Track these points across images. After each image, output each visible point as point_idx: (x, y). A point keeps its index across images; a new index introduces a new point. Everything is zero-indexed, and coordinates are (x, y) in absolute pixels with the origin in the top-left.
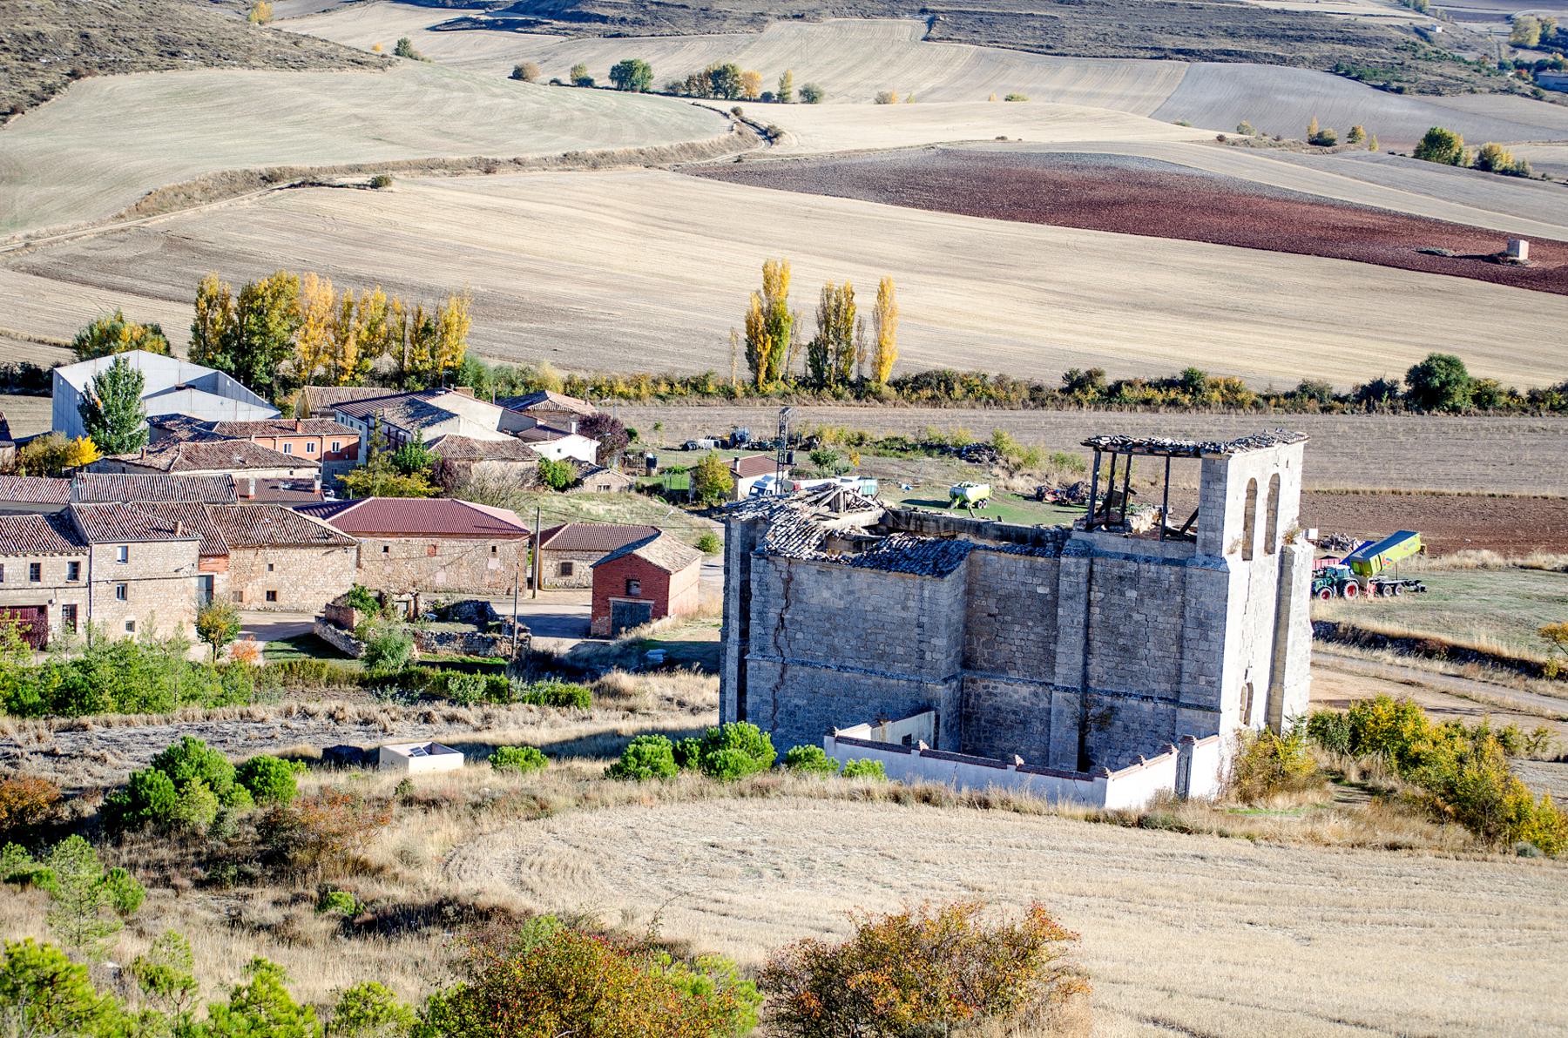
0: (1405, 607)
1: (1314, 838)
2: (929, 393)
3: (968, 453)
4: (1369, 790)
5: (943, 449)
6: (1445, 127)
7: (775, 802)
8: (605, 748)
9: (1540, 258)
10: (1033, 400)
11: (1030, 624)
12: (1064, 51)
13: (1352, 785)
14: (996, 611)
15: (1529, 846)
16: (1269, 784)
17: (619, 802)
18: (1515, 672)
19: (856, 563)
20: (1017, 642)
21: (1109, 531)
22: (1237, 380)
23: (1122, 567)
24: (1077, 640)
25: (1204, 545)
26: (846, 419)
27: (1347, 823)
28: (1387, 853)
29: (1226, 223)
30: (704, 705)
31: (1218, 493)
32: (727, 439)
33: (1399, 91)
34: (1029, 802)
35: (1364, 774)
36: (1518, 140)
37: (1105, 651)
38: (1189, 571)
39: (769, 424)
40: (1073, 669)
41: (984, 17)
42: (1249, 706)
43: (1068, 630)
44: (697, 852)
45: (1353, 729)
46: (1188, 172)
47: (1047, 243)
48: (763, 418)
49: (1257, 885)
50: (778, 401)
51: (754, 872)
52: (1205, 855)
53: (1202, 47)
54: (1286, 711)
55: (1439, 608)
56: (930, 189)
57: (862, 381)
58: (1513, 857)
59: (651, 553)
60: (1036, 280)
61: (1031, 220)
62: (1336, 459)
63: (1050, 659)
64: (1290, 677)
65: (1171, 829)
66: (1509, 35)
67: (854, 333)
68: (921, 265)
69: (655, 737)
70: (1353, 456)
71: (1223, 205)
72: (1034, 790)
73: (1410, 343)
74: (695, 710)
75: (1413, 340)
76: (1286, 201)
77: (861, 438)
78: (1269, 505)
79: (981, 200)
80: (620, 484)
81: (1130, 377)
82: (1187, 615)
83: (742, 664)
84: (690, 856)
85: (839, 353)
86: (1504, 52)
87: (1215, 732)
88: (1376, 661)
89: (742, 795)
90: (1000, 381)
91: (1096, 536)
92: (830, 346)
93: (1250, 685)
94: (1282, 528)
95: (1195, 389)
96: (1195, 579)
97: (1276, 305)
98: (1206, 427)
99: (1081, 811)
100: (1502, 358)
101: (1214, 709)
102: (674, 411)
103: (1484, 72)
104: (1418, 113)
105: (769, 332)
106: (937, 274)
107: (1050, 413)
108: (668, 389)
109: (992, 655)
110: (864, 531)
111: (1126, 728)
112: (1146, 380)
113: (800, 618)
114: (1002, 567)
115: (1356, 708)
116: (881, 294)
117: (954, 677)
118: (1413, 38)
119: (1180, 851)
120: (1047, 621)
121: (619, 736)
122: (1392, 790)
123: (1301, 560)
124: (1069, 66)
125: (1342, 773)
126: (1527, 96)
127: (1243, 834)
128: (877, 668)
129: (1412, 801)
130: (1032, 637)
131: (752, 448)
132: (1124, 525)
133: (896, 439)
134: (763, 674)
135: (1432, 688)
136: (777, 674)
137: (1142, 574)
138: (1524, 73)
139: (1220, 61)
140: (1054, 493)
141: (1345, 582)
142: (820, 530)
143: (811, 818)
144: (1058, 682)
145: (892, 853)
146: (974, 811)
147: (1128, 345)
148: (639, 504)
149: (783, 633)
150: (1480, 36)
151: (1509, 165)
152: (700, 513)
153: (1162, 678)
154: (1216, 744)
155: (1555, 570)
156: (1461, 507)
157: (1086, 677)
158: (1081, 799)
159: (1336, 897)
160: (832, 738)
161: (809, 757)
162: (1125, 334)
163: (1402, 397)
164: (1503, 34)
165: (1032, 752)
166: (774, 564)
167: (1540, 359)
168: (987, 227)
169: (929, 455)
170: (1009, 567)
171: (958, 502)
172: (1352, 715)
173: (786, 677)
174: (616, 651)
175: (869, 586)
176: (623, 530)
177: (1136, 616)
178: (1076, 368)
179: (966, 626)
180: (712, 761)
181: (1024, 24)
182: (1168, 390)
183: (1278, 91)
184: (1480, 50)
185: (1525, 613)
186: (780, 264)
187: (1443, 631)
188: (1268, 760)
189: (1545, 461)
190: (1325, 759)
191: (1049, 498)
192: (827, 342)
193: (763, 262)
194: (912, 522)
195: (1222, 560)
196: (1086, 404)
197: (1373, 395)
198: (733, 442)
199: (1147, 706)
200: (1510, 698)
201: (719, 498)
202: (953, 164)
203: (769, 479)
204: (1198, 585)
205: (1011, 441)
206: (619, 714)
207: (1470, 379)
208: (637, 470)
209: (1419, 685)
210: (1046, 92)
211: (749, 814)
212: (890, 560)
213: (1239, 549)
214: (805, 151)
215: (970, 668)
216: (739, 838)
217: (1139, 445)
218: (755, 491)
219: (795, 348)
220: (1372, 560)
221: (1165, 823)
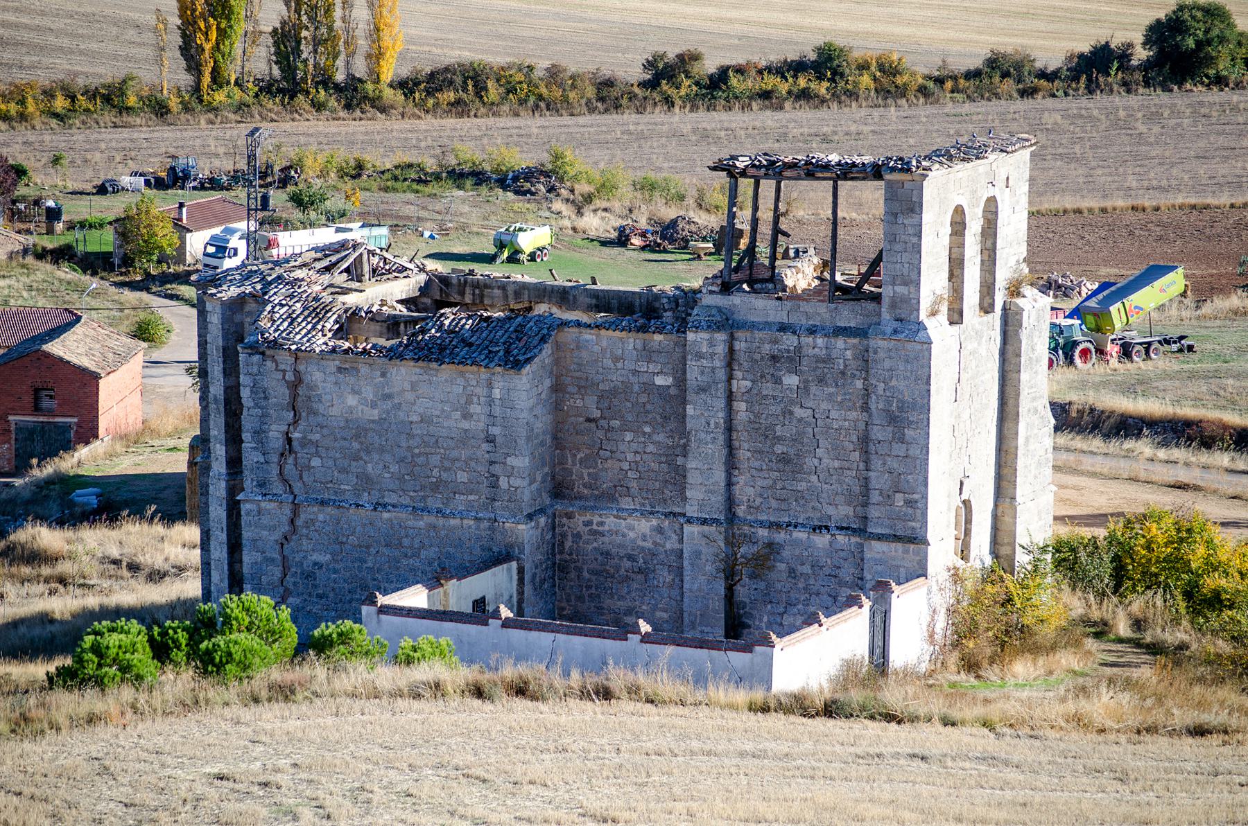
0: (1166, 375)
1: (1079, 721)
2: (451, 96)
4: (1148, 646)
5: (480, 177)
8: (32, 640)
10: (602, 99)
11: (647, 429)
13: (1120, 641)
14: (597, 414)
16: (1003, 645)
17: (74, 722)
19: (393, 354)
20: (630, 457)
21: (754, 291)
22: (895, 57)
23: (776, 342)
24: (716, 450)
25: (893, 306)
26: (333, 140)
27: (1125, 697)
28: (1190, 740)
30: (167, 567)
32: (164, 175)
34: (666, 686)
37: (757, 464)
38: (872, 343)
39: (221, 150)
40: (711, 492)
42: (967, 532)
43: (703, 436)
44: (199, 789)
45: (1116, 558)
48: (212, 142)
49: (1008, 794)
50: (231, 116)
51: (285, 814)
52: (927, 753)
54: (1022, 538)
55: (1217, 375)
59: (64, 348)
62: (1047, 164)
63: (678, 479)
64: (1023, 489)
65: (872, 718)
67: (338, 13)
69: (121, 622)
70: (1070, 158)
74: (156, 576)
77: (360, 167)
78: (983, 243)
80: (10, 248)
81: (740, 60)
82: (873, 407)
83: (233, 508)
84: (190, 796)
85: (317, 42)
87: (920, 571)
88: (1128, 455)
89: (256, 700)
90: (554, 73)
91: (736, 299)
92: (304, 33)
93: (967, 504)
94: (1003, 276)
95: (835, 73)
96: (881, 355)
98: (853, 128)
99: (741, 696)
101: (916, 540)
102: (78, 137)
107: (629, 119)
108: (67, 103)
109: (595, 477)
110: (399, 307)
111: (792, 572)
112: (763, 63)
113: (316, 437)
114: (604, 350)
115: (1118, 527)
117: (542, 511)
119: (890, 749)
120: (672, 425)
121: (52, 621)
122: (1183, 646)
123: (1033, 317)
125: (1106, 624)
127: (977, 720)
128: (430, 503)
129: (1214, 661)
130: (651, 448)
131: (202, 187)
132: (774, 280)
133: (410, 166)
134: (265, 520)
135: (1215, 492)
137: (805, 351)
140: (643, 235)
141: (1075, 344)
142: (338, 308)
143: (358, 728)
144: (691, 511)
145: (479, 772)
146: (589, 704)
148: (40, 276)
149: (291, 460)
152: (133, 286)
156: (1237, 224)
157: (730, 502)
158: (739, 680)
159: (1124, 809)
160: (373, 609)
161: (344, 638)
163: (1138, 68)
165: (659, 614)
166: (275, 361)
169: (459, 187)
171: (506, 254)
172: (1111, 539)
173: (299, 522)
174: (27, 494)
175: (414, 386)
176: (20, 316)
177: (799, 412)
178: (661, 50)
179: (555, 438)
180: (208, 652)
182: (795, 77)
187: (1224, 408)
188: (999, 610)
190: (1076, 604)
194: (468, 290)
195: (921, 326)
196: (678, 102)
198: (174, 179)
199: (822, 540)
201: (159, 262)
203: (233, 231)
204: (887, 364)
206: (41, 588)
207: (1241, 34)
208: (32, 226)
209: (1197, 488)
211: (269, 727)
212: (442, 349)
213: (944, 309)
215: (564, 497)
216: (258, 764)
217: (793, 166)
218: (211, 250)
219: (253, 37)
220: (1114, 309)
221: (863, 708)
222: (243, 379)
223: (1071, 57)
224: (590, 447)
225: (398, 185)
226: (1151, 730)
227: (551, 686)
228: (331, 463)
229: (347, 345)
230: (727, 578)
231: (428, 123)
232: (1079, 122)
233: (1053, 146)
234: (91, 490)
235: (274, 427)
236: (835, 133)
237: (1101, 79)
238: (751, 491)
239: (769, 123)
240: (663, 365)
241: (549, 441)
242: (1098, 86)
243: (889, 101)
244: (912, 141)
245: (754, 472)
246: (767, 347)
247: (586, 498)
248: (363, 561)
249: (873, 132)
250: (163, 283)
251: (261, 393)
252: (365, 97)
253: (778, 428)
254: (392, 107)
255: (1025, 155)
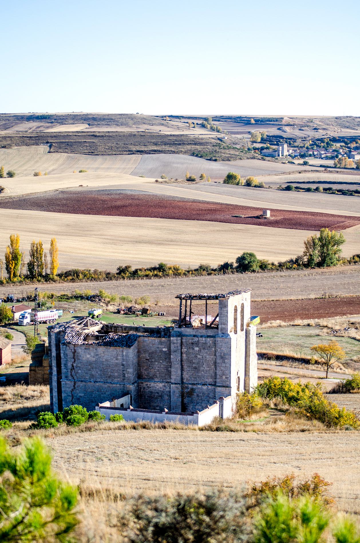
1: (275, 429)
2: (71, 278)
3: (91, 298)
4: (279, 410)
6: (234, 172)
7: (94, 433)
9: (274, 216)
10: (107, 278)
11: (161, 361)
12: (98, 154)
13: (272, 409)
14: (149, 358)
15: (349, 426)
18: (300, 363)
19: (98, 344)
20: (157, 368)
21: (186, 327)
22: (177, 266)
23: (193, 339)
24: (178, 366)
25: (221, 330)
28: (301, 433)
29: (163, 211)
31: (225, 312)
32: (6, 299)
33: (216, 160)
35: (275, 405)
36: (258, 175)
37: (189, 369)
38: (217, 339)
39: (17, 292)
40: (177, 376)
41: (69, 143)
42: (239, 384)
43: (175, 363)
46: (148, 193)
47: (102, 222)
48: (14, 291)
50: (18, 284)
52: (244, 439)
53: (146, 149)
54: (251, 385)
56: (59, 205)
57: (47, 275)
58: (344, 431)
60: (101, 235)
61: (95, 214)
63: (169, 373)
66: (250, 138)
67: (43, 258)
68: (60, 232)
71: (162, 204)
72: (181, 421)
73: (234, 249)
75: (235, 247)
76: (183, 201)
77: (52, 296)
79: (77, 208)
81: (140, 267)
82: (217, 355)
85: (38, 266)
86: (249, 145)
87: (230, 394)
89: (82, 431)
90: (95, 272)
92: (35, 264)
93: (239, 378)
96: (219, 342)
97: (185, 239)
100: (266, 252)
101: (229, 387)
103: (244, 152)
104: (222, 168)
105: (13, 260)
106: (66, 235)
107: (114, 282)
109: (148, 373)
111: (198, 396)
112: (146, 268)
113: (79, 365)
114: (150, 343)
115: (267, 381)
116: (52, 244)
117: (135, 382)
118: (218, 142)
121: (13, 411)
122: (287, 410)
124: (100, 159)
125: (268, 405)
126: (260, 159)
127: (252, 430)
128: (108, 381)
130: (162, 366)
133: (65, 295)
134: (67, 386)
136: (72, 385)
137: (200, 341)
138: (257, 151)
139: (152, 154)
140: (124, 311)
144: (173, 381)
147: (137, 256)
149: (73, 371)
150: (240, 139)
151: (257, 184)
153: (209, 377)
154: (231, 399)
155: (304, 326)
157: (182, 379)
160: (98, 407)
162: (135, 252)
163: (235, 268)
164: (248, 138)
166: (69, 347)
167: (280, 251)
168: (81, 217)
169: (77, 300)
170: (152, 342)
171: (91, 316)
173: (76, 386)
175: (103, 352)
177: (199, 356)
179: (138, 364)
181: (83, 145)
182: (154, 271)
183: (173, 163)
184: (241, 144)
185: (299, 342)
186: (16, 236)
188: (247, 403)
189: (288, 287)
191: (122, 312)
192: (34, 262)
193: (9, 236)
195: (228, 335)
196: (126, 278)
197: (225, 268)
199: (205, 387)
200: (301, 372)
201: (8, 320)
202: (65, 196)
203: (26, 312)
204: (220, 344)
205: (106, 293)
207: (258, 260)
209: (269, 370)
210: (93, 168)
213: (233, 330)
214: (13, 195)
217: (194, 297)
218: (21, 317)
221: (225, 429)
222: (61, 351)
223: (219, 266)
224: (147, 366)
225: (62, 300)
226: (292, 431)
227: (151, 426)
228: (83, 371)
229: (87, 343)
230: (182, 398)
231: (66, 284)
232: (222, 281)
233: (217, 287)
234: (4, 377)
235: (69, 363)
236: (165, 285)
237: (226, 271)
238: (187, 376)
239: (148, 282)
240: (165, 346)
241: (137, 365)
242: (226, 272)
243: (177, 277)
244: (183, 286)
245: (188, 371)
246: (191, 341)
247: (146, 379)
248: (92, 395)
249: (174, 284)
250: (9, 326)
251: (66, 355)
252: (50, 279)
253: (194, 360)
254: (57, 281)
255: (249, 293)
